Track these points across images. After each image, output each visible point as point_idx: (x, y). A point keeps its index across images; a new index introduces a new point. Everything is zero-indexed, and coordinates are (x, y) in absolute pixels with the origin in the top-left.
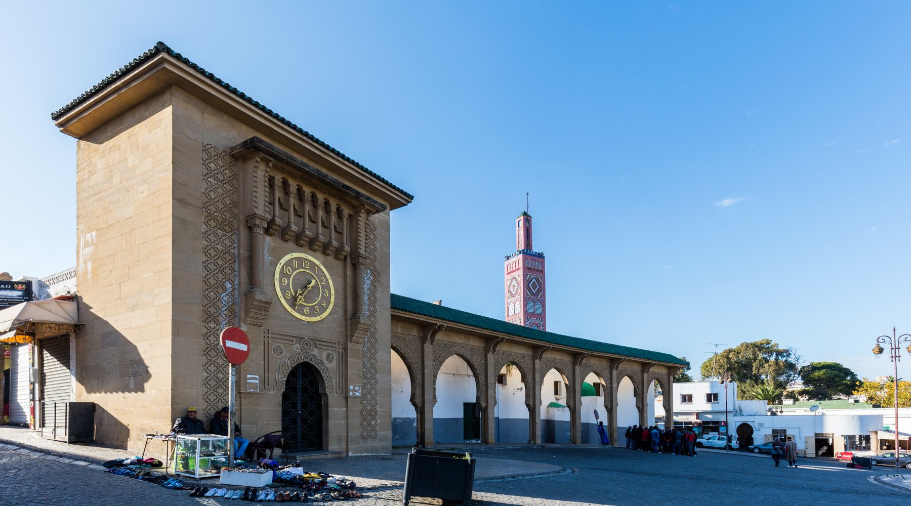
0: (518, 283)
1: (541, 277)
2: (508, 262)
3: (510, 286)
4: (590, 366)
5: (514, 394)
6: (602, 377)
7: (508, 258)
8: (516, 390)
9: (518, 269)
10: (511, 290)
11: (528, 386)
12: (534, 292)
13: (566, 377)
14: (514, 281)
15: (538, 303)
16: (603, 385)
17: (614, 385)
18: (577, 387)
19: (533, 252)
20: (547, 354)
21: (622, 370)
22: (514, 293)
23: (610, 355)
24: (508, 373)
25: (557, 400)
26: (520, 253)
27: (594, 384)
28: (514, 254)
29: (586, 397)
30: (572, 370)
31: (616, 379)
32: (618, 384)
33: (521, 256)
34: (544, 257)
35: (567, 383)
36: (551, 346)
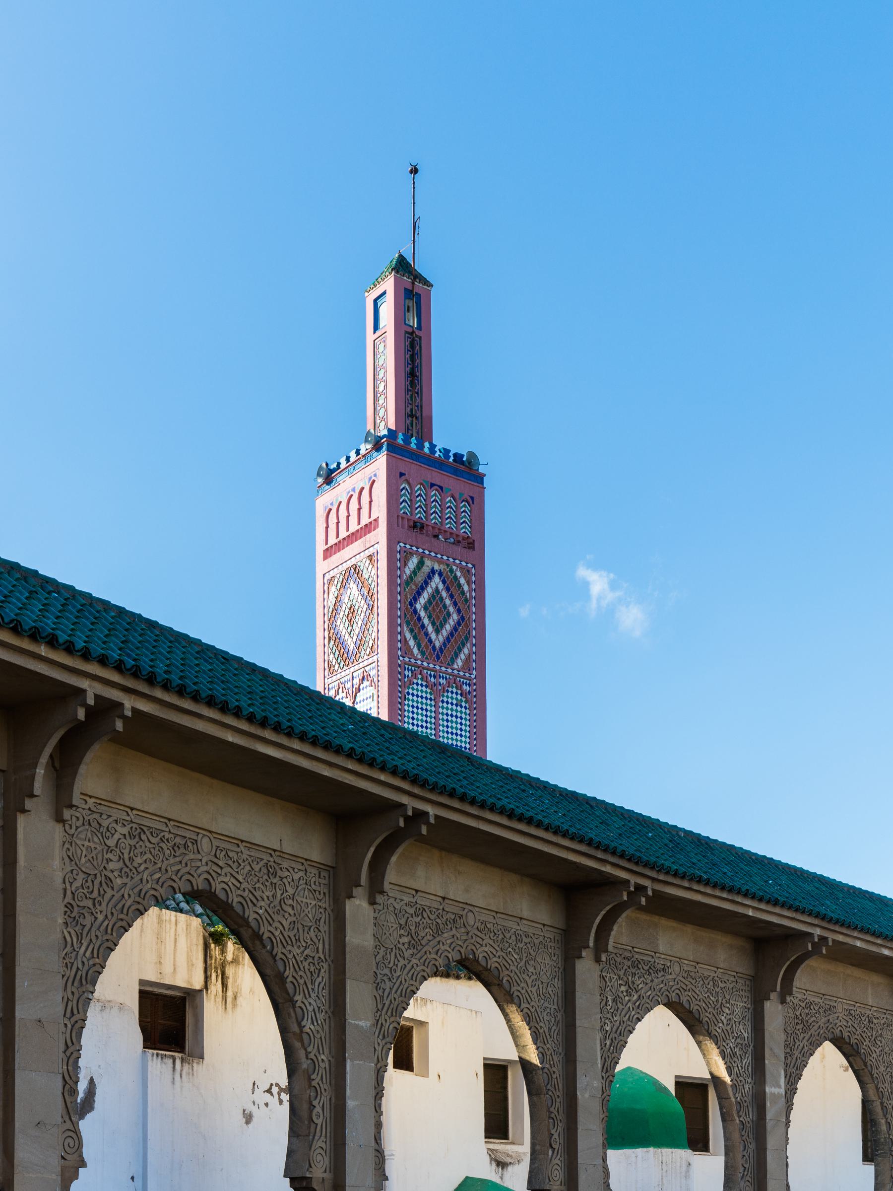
0: (370, 596)
1: (466, 572)
2: (327, 498)
3: (335, 609)
4: (652, 969)
5: (248, 1118)
6: (710, 1035)
7: (329, 477)
8: (261, 1097)
9: (368, 528)
10: (342, 627)
11: (305, 1064)
12: (438, 641)
13: (528, 1019)
14: (352, 586)
15: (453, 696)
16: (466, 596)
17: (775, 1089)
18: (582, 1081)
19: (433, 447)
20: (421, 872)
21: (809, 1005)
22: (351, 645)
23: (751, 910)
24: (216, 986)
25: (501, 1165)
26: (377, 447)
27: (682, 1085)
28: (353, 458)
29: (640, 1151)
30: (557, 983)
31: (781, 1053)
32: (791, 1090)
33: (381, 461)
34: (479, 479)
35: (533, 1057)
36: (431, 810)
